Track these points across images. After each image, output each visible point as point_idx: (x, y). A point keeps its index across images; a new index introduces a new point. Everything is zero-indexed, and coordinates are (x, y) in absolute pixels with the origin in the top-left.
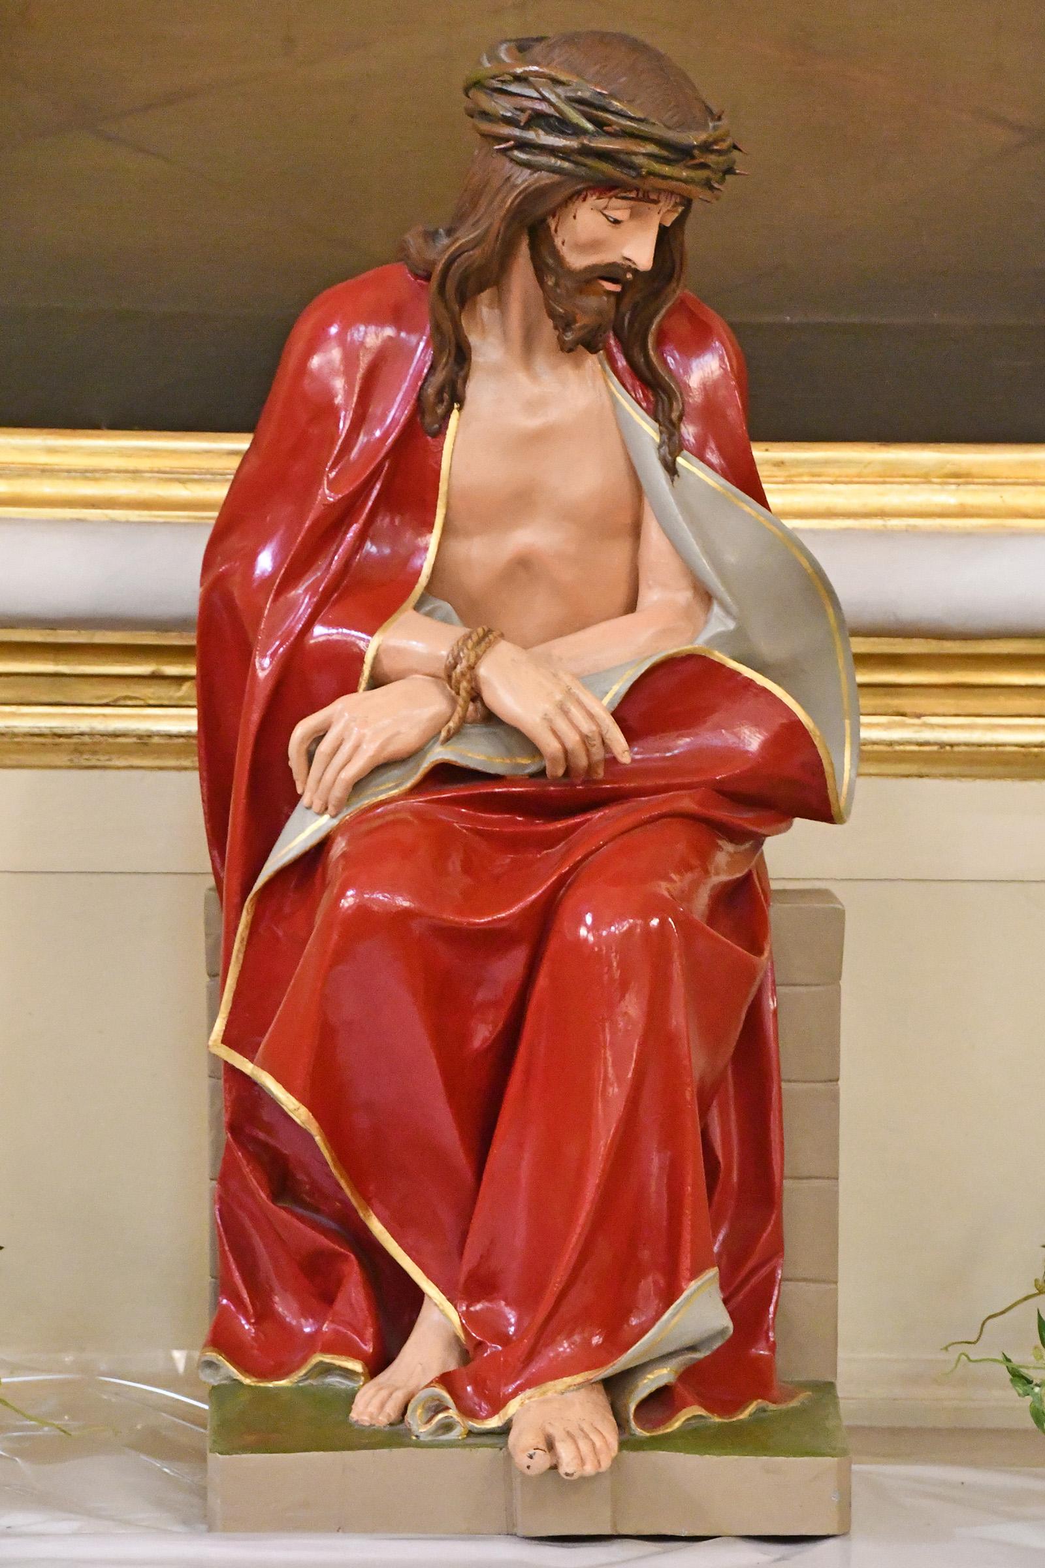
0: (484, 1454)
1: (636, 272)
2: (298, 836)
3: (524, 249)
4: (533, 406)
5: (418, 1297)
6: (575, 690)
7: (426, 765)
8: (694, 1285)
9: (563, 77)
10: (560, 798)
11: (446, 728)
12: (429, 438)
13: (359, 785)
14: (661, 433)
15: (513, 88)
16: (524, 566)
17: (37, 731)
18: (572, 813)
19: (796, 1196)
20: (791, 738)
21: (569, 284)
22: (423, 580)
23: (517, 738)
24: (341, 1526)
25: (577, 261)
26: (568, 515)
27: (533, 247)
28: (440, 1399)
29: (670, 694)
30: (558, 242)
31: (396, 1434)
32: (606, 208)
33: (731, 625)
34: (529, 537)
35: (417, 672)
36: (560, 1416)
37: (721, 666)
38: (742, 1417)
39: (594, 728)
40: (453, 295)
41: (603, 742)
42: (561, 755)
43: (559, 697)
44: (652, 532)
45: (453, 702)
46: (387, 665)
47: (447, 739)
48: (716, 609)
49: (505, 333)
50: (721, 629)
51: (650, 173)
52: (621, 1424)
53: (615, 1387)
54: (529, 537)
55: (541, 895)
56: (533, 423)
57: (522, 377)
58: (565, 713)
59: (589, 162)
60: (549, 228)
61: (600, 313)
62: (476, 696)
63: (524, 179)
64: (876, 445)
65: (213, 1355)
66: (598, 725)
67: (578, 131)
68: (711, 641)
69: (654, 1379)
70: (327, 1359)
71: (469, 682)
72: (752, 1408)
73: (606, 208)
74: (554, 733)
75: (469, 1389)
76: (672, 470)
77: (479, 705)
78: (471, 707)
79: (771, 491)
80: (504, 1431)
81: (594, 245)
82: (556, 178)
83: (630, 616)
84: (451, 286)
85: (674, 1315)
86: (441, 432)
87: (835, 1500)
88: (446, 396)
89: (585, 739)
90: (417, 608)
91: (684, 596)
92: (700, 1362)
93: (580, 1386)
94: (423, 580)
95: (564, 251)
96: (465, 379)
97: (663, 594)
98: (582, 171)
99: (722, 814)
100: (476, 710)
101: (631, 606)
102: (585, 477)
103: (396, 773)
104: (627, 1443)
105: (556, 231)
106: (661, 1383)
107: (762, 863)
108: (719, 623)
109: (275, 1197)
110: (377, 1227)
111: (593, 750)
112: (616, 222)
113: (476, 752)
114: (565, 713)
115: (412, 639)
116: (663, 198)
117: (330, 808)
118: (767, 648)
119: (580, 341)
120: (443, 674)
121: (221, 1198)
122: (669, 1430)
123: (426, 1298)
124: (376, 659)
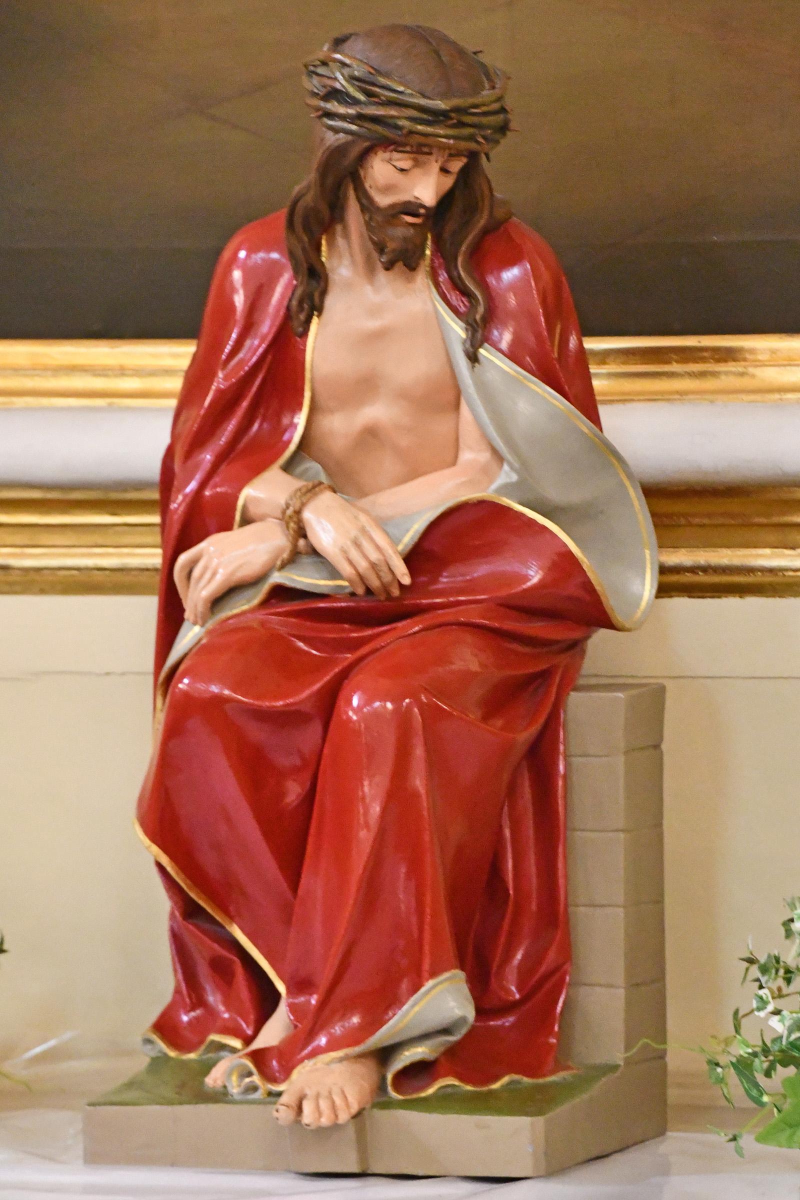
1: (423, 207)
4: (374, 311)
6: (368, 528)
7: (265, 588)
8: (430, 983)
9: (348, 61)
10: (370, 611)
12: (298, 339)
13: (217, 602)
14: (467, 330)
15: (320, 70)
16: (371, 435)
17: (144, 567)
20: (566, 564)
21: (379, 218)
24: (173, 1162)
25: (383, 201)
26: (403, 395)
27: (355, 190)
30: (367, 185)
31: (221, 1096)
33: (514, 477)
34: (377, 412)
35: (269, 516)
36: (329, 1082)
37: (508, 509)
39: (381, 557)
40: (311, 227)
43: (354, 532)
44: (464, 408)
46: (253, 511)
48: (506, 467)
49: (352, 256)
50: (508, 480)
51: (411, 132)
56: (373, 324)
57: (368, 289)
58: (357, 544)
59: (366, 125)
61: (405, 239)
62: (301, 532)
63: (331, 139)
64: (783, 336)
65: (155, 1037)
66: (383, 555)
67: (356, 102)
68: (499, 491)
71: (295, 523)
72: (506, 1079)
73: (391, 159)
74: (350, 562)
75: (274, 1063)
76: (473, 358)
79: (598, 375)
81: (388, 189)
82: (350, 138)
84: (298, 221)
86: (305, 334)
87: (531, 1150)
88: (306, 306)
89: (373, 566)
90: (287, 468)
91: (485, 456)
92: (458, 1043)
93: (341, 1060)
94: (292, 447)
95: (373, 193)
96: (324, 293)
97: (472, 455)
98: (363, 130)
99: (510, 625)
101: (454, 462)
102: (412, 366)
111: (382, 574)
112: (402, 170)
115: (267, 491)
116: (435, 151)
118: (555, 494)
119: (403, 260)
120: (280, 516)
121: (456, 934)
124: (245, 507)
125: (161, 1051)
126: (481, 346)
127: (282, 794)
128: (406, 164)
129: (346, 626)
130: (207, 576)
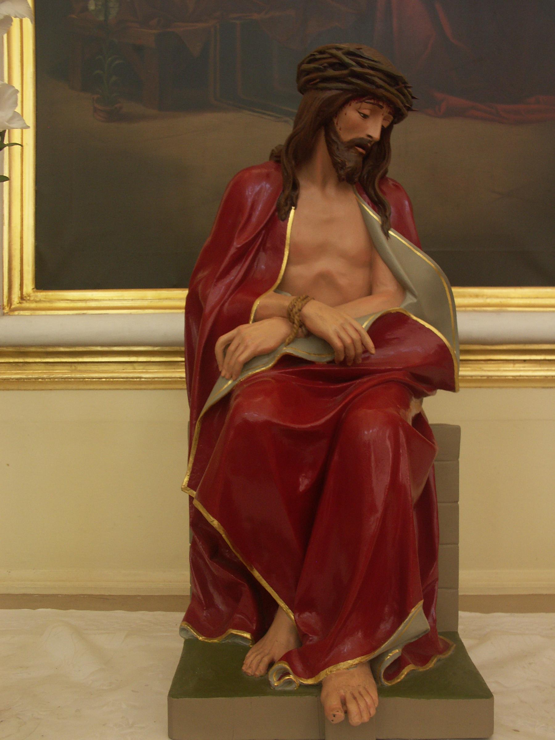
0: (308, 699)
2: (223, 387)
3: (323, 133)
5: (277, 605)
7: (278, 356)
11: (288, 338)
13: (247, 364)
18: (346, 381)
19: (442, 550)
22: (278, 282)
23: (325, 343)
25: (347, 137)
27: (327, 136)
28: (285, 669)
29: (386, 327)
30: (338, 129)
31: (260, 687)
32: (359, 108)
33: (415, 300)
34: (323, 264)
38: (430, 666)
41: (362, 344)
42: (342, 349)
45: (292, 327)
47: (289, 344)
52: (376, 678)
53: (373, 665)
54: (323, 264)
55: (334, 415)
60: (334, 123)
62: (302, 324)
69: (393, 655)
70: (234, 632)
71: (299, 316)
73: (359, 108)
76: (387, 235)
77: (304, 329)
78: (300, 330)
80: (319, 686)
83: (369, 297)
85: (405, 626)
89: (353, 340)
94: (278, 282)
98: (350, 87)
100: (302, 332)
103: (266, 360)
104: (382, 691)
105: (337, 124)
106: (396, 657)
107: (422, 409)
108: (410, 300)
109: (211, 557)
110: (256, 574)
113: (300, 350)
114: (345, 329)
117: (234, 376)
122: (399, 680)
123: (279, 610)
125: (193, 636)
126: (389, 229)
127: (298, 485)
128: (367, 112)
129: (321, 382)
130: (241, 349)
